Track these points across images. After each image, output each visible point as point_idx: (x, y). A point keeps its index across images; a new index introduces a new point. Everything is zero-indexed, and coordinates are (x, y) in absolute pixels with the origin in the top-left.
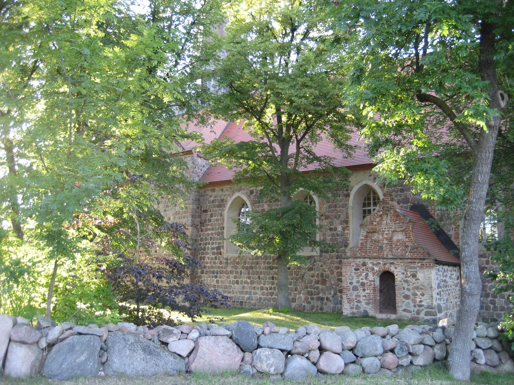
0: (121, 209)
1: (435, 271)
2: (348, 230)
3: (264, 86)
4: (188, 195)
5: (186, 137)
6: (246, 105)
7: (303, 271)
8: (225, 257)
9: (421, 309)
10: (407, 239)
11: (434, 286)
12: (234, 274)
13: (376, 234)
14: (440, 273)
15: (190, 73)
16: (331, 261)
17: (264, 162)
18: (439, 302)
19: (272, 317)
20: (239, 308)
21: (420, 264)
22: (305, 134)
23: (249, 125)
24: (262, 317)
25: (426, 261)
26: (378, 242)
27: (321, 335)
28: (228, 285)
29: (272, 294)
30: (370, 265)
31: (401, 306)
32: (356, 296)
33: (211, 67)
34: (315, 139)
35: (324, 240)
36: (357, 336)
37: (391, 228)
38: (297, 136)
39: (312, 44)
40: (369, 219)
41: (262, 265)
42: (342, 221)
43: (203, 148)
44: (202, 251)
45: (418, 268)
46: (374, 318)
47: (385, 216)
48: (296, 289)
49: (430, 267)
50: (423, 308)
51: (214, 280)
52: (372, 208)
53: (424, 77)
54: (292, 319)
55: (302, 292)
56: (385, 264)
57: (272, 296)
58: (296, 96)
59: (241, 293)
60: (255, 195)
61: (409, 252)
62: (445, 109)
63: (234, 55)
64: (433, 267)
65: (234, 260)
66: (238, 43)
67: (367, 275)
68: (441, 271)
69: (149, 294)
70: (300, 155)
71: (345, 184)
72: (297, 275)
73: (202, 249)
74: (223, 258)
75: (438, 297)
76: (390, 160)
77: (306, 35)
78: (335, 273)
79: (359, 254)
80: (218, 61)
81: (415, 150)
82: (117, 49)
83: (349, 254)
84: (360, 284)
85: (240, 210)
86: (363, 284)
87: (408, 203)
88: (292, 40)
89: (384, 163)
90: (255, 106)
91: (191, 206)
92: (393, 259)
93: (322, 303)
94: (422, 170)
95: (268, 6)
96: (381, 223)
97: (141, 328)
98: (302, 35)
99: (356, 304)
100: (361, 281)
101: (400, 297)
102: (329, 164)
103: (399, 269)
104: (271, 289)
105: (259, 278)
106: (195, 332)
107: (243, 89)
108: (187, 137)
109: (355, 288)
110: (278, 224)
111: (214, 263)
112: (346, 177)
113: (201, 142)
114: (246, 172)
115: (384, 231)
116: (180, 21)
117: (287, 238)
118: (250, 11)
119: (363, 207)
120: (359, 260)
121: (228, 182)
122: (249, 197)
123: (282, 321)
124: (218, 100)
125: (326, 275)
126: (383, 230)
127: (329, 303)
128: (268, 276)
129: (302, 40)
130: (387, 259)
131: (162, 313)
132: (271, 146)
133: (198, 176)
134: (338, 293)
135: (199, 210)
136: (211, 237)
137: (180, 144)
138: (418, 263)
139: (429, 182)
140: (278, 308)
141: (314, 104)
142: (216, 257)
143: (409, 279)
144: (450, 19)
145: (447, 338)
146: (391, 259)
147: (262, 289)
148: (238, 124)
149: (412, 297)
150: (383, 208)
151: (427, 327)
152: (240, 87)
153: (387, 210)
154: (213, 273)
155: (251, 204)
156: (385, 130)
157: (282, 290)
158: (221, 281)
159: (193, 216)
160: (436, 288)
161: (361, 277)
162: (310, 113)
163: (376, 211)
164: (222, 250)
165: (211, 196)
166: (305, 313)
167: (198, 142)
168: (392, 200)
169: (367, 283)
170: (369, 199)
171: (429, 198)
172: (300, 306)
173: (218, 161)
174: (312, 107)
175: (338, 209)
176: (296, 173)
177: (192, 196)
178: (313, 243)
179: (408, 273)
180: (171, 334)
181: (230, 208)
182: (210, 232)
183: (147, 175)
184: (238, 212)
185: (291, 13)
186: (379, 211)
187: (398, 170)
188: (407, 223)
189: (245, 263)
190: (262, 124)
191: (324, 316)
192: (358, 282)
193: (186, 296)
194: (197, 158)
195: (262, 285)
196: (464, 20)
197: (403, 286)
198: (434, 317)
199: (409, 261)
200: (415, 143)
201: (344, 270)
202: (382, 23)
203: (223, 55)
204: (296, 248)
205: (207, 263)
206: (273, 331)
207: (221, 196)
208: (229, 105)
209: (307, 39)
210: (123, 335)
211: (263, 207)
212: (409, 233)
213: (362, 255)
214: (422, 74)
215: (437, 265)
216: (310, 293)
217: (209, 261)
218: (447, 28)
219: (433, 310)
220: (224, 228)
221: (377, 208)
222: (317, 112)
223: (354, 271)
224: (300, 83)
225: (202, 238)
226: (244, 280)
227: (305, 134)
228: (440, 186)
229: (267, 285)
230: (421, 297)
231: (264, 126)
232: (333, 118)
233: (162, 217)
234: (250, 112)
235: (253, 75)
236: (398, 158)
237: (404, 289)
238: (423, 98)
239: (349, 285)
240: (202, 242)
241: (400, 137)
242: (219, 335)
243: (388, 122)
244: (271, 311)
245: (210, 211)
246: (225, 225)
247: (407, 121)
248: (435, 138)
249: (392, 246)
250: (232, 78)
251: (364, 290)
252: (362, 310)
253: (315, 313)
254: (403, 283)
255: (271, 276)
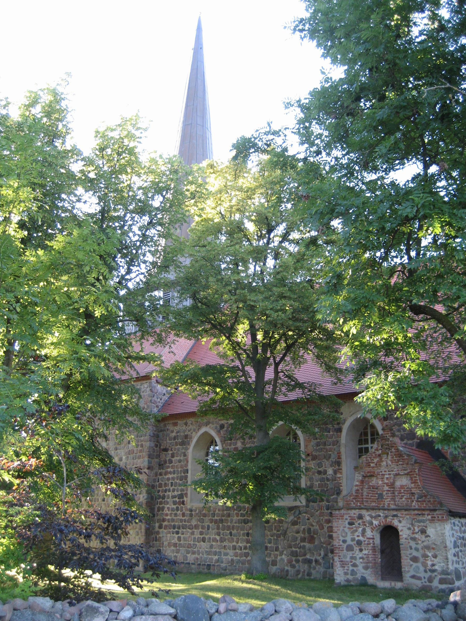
0: (38, 448)
1: (449, 525)
2: (341, 473)
3: (233, 298)
4: (145, 430)
5: (141, 359)
6: (213, 320)
7: (285, 525)
8: (189, 507)
9: (434, 575)
10: (413, 485)
11: (450, 544)
12: (200, 530)
13: (374, 479)
14: (457, 528)
15: (145, 282)
16: (321, 513)
17: (235, 390)
18: (457, 566)
19: (245, 585)
20: (206, 573)
21: (430, 517)
22: (285, 355)
23: (218, 344)
24: (231, 586)
25: (437, 512)
26: (377, 489)
27: (294, 613)
28: (192, 543)
29: (247, 555)
30: (368, 518)
31: (409, 571)
32: (352, 558)
33: (172, 276)
34: (298, 361)
35: (311, 486)
36: (341, 615)
37: (393, 471)
38: (274, 358)
39: (293, 248)
40: (365, 459)
41: (235, 518)
42: (332, 462)
43: (161, 372)
44: (161, 500)
45: (428, 522)
46: (374, 587)
47: (385, 456)
48: (277, 549)
49: (442, 520)
50: (436, 574)
51: (174, 537)
52: (369, 445)
53: (415, 284)
54: (270, 589)
55: (285, 552)
56: (386, 517)
57: (247, 557)
58: (271, 309)
59: (208, 553)
60: (226, 431)
61: (417, 501)
62: (444, 324)
63: (197, 261)
64: (447, 520)
65: (200, 512)
66: (204, 246)
67: (364, 531)
68: (458, 526)
69: (75, 558)
70: (280, 381)
71: (333, 417)
72: (278, 531)
73: (160, 497)
74: (187, 509)
75: (455, 559)
76: (377, 387)
77: (285, 237)
78: (326, 529)
79: (354, 503)
80: (179, 267)
81: (407, 374)
82: (40, 252)
83: (341, 504)
84: (355, 542)
85: (208, 449)
86: (359, 543)
87: (413, 439)
88: (268, 243)
89: (369, 391)
90: (225, 322)
91: (148, 444)
92: (396, 510)
93: (310, 567)
94: (416, 399)
95: (239, 203)
96: (380, 465)
97: (59, 605)
98: (280, 237)
99: (351, 568)
100: (357, 538)
101: (407, 559)
102: (314, 392)
103: (404, 522)
104: (245, 548)
105: (231, 534)
106: (128, 610)
107: (210, 301)
108: (143, 359)
109: (350, 548)
110: (252, 467)
111: (176, 515)
112: (336, 409)
113: (159, 365)
114: (213, 401)
115: (384, 475)
116: (134, 221)
117: (263, 484)
118: (218, 209)
119: (359, 445)
120: (354, 511)
121: (192, 414)
122: (218, 432)
123: (256, 590)
124: (178, 314)
125: (314, 530)
126: (383, 473)
127: (319, 566)
128: (242, 532)
129: (281, 242)
130: (388, 510)
131: (91, 583)
132: (243, 370)
133: (157, 407)
134: (330, 554)
135: (158, 448)
136: (172, 483)
137: (134, 367)
138: (428, 515)
139: (425, 415)
140: (252, 574)
141: (295, 319)
142: (177, 508)
143: (417, 536)
144: (443, 215)
145: (460, 618)
146: (393, 510)
147: (234, 548)
148: (203, 343)
149: (421, 559)
150: (382, 446)
151: (434, 602)
152: (206, 298)
153: (387, 448)
154: (174, 527)
155: (221, 441)
156: (371, 349)
157: (257, 550)
158: (184, 538)
159: (150, 456)
160: (452, 547)
161: (357, 534)
162: (290, 330)
163: (373, 450)
164: (185, 499)
165: (172, 432)
166: (289, 580)
167: (156, 366)
168: (393, 435)
169: (365, 541)
170: (366, 434)
171: (426, 435)
172: (283, 570)
173: (180, 388)
174: (291, 322)
175: (328, 447)
176: (274, 402)
177: (148, 431)
178: (297, 490)
179: (416, 528)
180: (96, 613)
181: (195, 446)
182: (170, 476)
183: (90, 405)
184: (206, 451)
185: (266, 211)
186: (377, 450)
187: (386, 399)
188: (412, 464)
189: (214, 515)
190: (233, 343)
191: (312, 584)
192: (353, 540)
193: (119, 560)
194: (156, 385)
195: (234, 543)
196: (459, 215)
197: (411, 544)
198: (450, 586)
199: (416, 512)
200: (407, 366)
201: (335, 524)
202: (361, 220)
203: (186, 261)
204: (275, 497)
205: (167, 515)
206: (230, 608)
207: (184, 431)
208: (191, 320)
209: (287, 241)
210: (33, 614)
211: (236, 444)
212: (415, 477)
213: (357, 505)
214: (413, 281)
215: (452, 518)
216: (294, 554)
217: (170, 512)
218: (439, 225)
219: (449, 577)
220: (187, 470)
221: (375, 446)
222: (297, 328)
223: (347, 526)
224: (276, 294)
225: (161, 484)
226: (211, 537)
227: (285, 355)
228: (441, 419)
229: (241, 543)
230: (433, 559)
231: (236, 346)
232: (318, 335)
233: (110, 457)
234: (217, 329)
235: (220, 284)
236: (386, 384)
237: (411, 548)
238: (417, 310)
239: (341, 543)
240: (161, 489)
241: (391, 358)
242: (159, 614)
243: (374, 340)
244: (243, 577)
245: (171, 450)
246: (189, 467)
247: (397, 339)
248: (443, 358)
249: (394, 493)
250: (195, 288)
251: (361, 550)
252: (359, 576)
253: (300, 580)
254: (410, 541)
255: (246, 532)
